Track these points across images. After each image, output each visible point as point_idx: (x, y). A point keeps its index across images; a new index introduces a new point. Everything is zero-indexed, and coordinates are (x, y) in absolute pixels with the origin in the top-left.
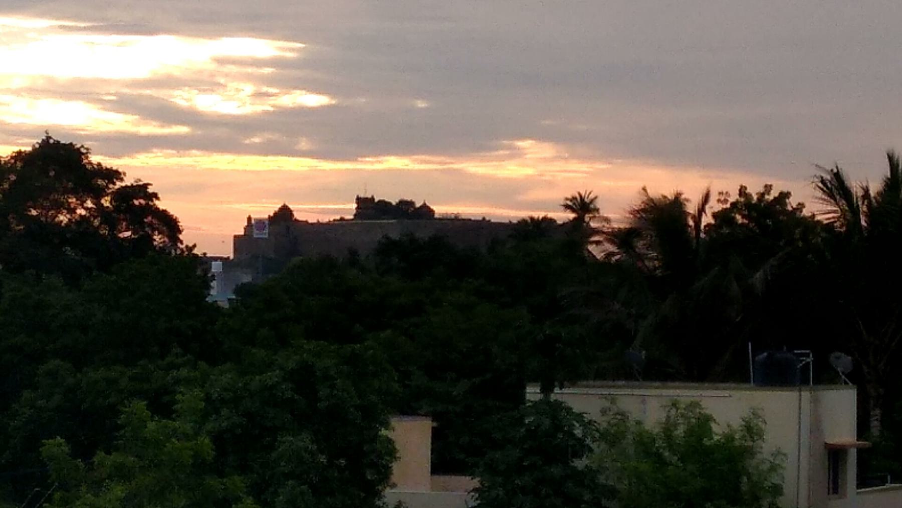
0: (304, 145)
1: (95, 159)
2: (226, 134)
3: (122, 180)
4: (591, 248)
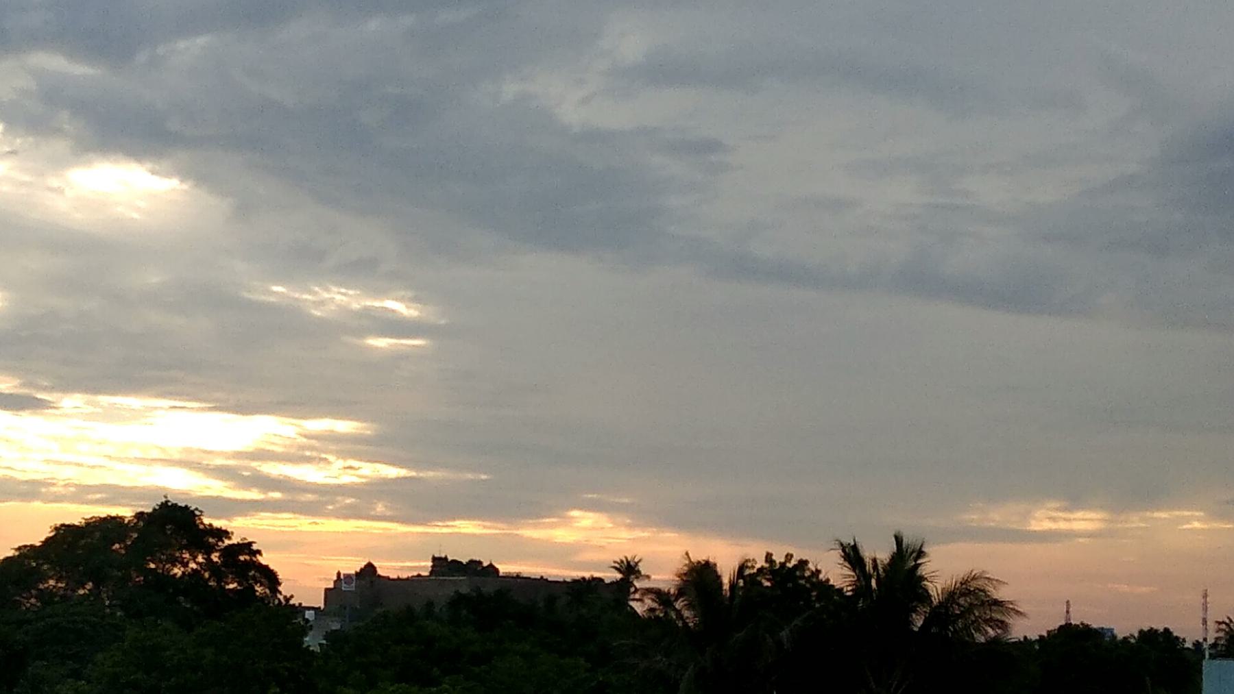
0: (380, 508)
1: (206, 521)
2: (299, 499)
3: (230, 538)
4: (631, 603)
